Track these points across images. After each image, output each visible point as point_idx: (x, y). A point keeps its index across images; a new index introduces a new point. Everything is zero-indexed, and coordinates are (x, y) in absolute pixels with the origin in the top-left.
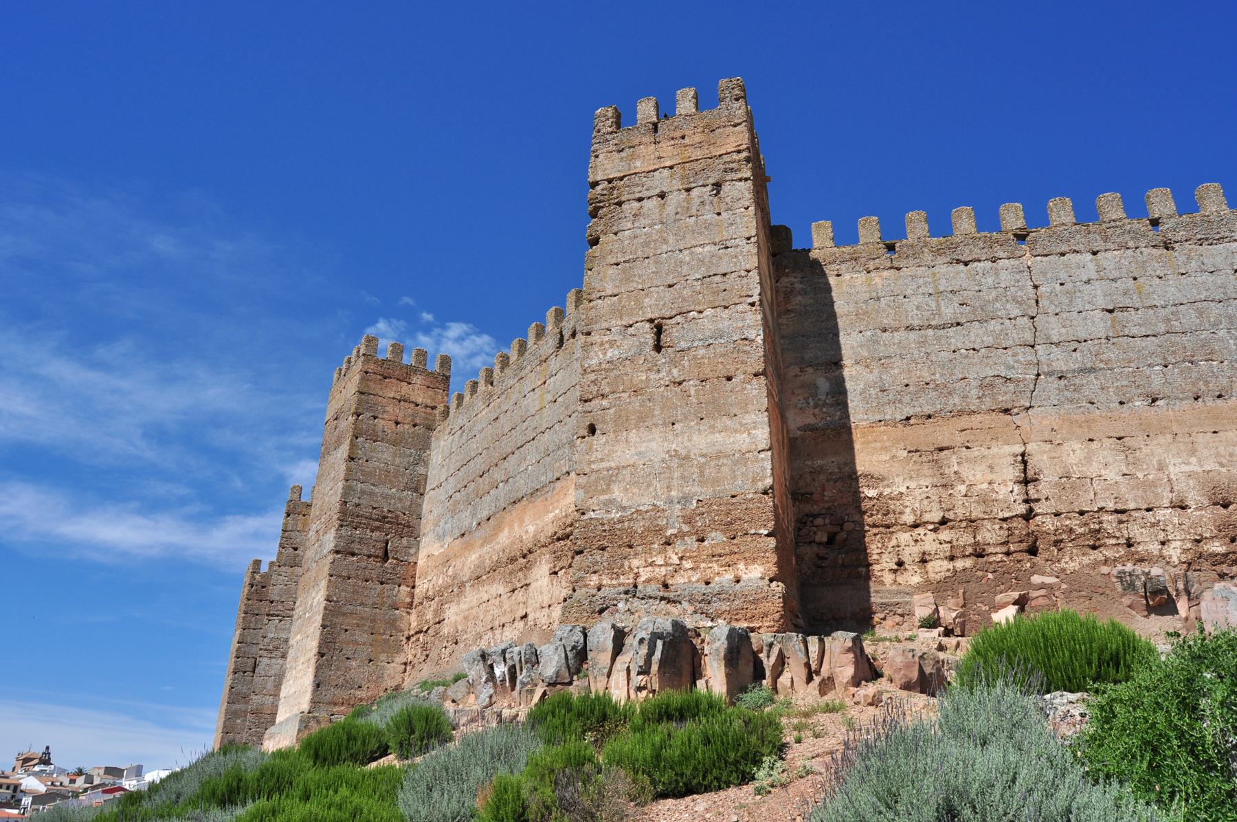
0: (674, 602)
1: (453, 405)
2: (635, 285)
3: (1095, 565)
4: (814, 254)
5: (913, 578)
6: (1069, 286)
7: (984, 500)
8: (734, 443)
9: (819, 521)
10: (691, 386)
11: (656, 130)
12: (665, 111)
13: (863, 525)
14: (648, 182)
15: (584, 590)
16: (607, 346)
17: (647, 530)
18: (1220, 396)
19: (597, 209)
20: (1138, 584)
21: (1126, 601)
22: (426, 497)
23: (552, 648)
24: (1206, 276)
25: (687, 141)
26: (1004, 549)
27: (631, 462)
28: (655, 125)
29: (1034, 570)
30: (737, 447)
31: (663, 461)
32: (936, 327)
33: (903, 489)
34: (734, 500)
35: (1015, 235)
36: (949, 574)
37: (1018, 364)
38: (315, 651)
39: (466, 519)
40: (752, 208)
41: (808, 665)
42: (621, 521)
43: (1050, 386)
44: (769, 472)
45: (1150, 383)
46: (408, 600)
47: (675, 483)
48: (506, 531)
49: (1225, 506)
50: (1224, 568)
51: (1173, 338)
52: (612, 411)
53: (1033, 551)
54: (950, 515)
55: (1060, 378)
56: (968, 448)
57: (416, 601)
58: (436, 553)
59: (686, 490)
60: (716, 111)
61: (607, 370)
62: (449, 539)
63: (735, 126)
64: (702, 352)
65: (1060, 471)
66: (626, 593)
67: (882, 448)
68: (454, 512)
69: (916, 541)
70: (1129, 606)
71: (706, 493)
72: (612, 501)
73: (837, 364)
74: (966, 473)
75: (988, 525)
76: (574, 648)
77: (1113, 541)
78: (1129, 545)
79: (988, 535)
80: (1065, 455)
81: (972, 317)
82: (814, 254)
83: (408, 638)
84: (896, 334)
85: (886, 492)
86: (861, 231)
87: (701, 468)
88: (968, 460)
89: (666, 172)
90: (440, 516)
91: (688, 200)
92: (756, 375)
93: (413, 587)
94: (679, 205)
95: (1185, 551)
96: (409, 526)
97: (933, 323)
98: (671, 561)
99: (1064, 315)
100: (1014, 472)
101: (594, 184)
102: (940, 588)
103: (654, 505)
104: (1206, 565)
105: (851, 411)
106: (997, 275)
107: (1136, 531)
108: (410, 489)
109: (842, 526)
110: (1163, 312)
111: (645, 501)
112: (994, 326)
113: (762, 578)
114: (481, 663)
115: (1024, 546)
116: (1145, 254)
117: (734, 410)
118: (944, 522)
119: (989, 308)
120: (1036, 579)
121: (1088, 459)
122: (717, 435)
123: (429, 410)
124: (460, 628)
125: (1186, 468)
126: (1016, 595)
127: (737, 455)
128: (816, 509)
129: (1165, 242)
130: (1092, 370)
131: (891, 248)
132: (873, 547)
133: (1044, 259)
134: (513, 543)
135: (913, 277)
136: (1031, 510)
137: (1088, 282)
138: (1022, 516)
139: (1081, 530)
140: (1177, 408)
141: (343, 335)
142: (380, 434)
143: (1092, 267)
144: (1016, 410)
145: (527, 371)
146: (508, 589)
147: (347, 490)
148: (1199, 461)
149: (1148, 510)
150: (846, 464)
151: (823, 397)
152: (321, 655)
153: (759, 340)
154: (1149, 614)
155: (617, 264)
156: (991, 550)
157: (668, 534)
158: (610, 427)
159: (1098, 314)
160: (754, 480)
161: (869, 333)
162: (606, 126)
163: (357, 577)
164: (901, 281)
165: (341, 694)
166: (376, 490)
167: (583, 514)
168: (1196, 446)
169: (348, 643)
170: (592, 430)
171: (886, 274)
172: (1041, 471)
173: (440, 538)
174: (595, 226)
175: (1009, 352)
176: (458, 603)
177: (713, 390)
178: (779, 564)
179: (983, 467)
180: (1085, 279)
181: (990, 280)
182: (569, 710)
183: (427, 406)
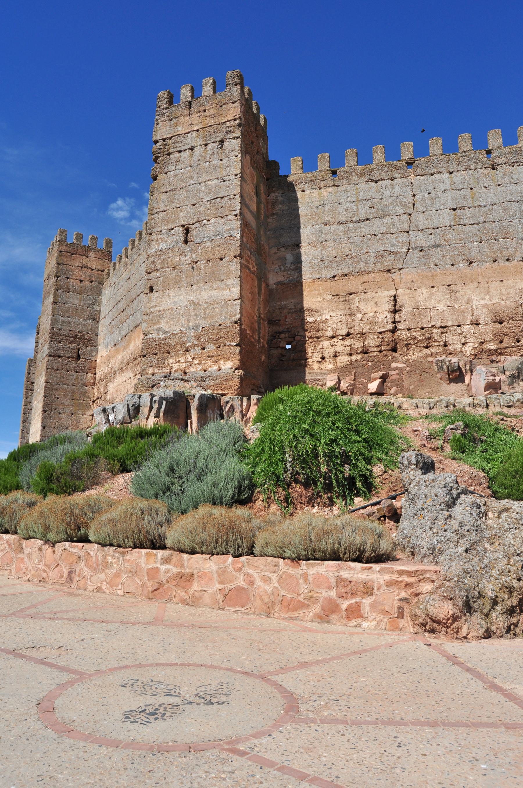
0: (188, 381)
1: (112, 268)
3: (426, 356)
4: (290, 179)
5: (329, 365)
6: (433, 194)
7: (371, 322)
8: (222, 296)
9: (282, 336)
10: (202, 264)
11: (190, 107)
12: (195, 93)
13: (305, 337)
14: (185, 141)
15: (146, 376)
16: (160, 241)
17: (177, 343)
18: (508, 260)
19: (157, 158)
20: (445, 367)
21: (439, 376)
22: (100, 323)
23: (122, 405)
24: (513, 187)
25: (207, 113)
26: (379, 349)
27: (170, 307)
29: (393, 360)
30: (223, 298)
31: (186, 306)
32: (355, 222)
33: (328, 317)
34: (220, 327)
35: (407, 163)
36: (348, 363)
37: (397, 244)
38: (41, 409)
39: (117, 337)
41: (242, 411)
42: (164, 339)
43: (415, 255)
44: (238, 311)
45: (470, 253)
46: (92, 381)
47: (192, 318)
48: (133, 343)
49: (501, 323)
50: (494, 357)
51: (488, 225)
53: (394, 350)
54: (352, 331)
55: (421, 251)
56: (365, 293)
57: (97, 382)
58: (105, 355)
59: (197, 322)
60: (223, 93)
61: (160, 255)
62: (109, 347)
63: (233, 103)
64: (208, 244)
65: (413, 305)
66: (165, 377)
67: (318, 294)
68: (112, 332)
69: (333, 345)
70: (440, 379)
71: (206, 323)
72: (160, 329)
73: (298, 245)
74: (363, 308)
75: (371, 336)
76: (133, 405)
77: (437, 344)
78: (446, 346)
79: (371, 341)
80: (417, 296)
81: (376, 215)
82: (290, 179)
83: (93, 402)
84: (332, 226)
85: (319, 318)
86: (319, 163)
87: (205, 309)
88: (365, 300)
89: (194, 134)
90: (106, 334)
91: (205, 152)
92: (235, 257)
93: (95, 374)
94: (200, 155)
95: (474, 348)
96: (91, 340)
97: (354, 219)
98: (188, 360)
99: (427, 213)
100: (389, 306)
101: (156, 142)
102: (342, 371)
104: (485, 356)
105: (303, 273)
106: (393, 188)
107: (450, 338)
108: (91, 319)
109: (294, 338)
110: (484, 209)
111: (176, 328)
112: (388, 220)
113: (231, 368)
114: (103, 414)
115: (389, 347)
116: (480, 173)
117: (223, 277)
118: (348, 335)
119: (386, 209)
120: (394, 365)
121: (430, 298)
122: (214, 291)
123: (100, 272)
124: (114, 396)
125: (482, 302)
126: (381, 374)
127: (223, 302)
128: (281, 329)
129: (493, 165)
130: (439, 245)
131: (334, 173)
132: (309, 349)
133: (421, 178)
134: (135, 349)
135: (345, 191)
136: (396, 327)
137: (444, 192)
138: (390, 331)
139: (421, 338)
140: (483, 267)
141: (96, 210)
142: (71, 287)
143: (448, 182)
144: (393, 271)
145: (141, 250)
147: (54, 321)
148: (490, 298)
149: (458, 326)
150: (298, 303)
151: (289, 265)
152: (44, 411)
154: (450, 383)
155: (166, 192)
156: (371, 349)
157: (187, 346)
159: (447, 211)
160: (231, 316)
161: (317, 226)
162: (163, 104)
163: (62, 369)
164: (338, 194)
166: (71, 320)
167: (146, 335)
168: (490, 289)
169: (59, 405)
170: (151, 289)
171: (330, 189)
172: (403, 305)
173: (106, 346)
174: (156, 168)
175: (394, 236)
177: (213, 266)
178: (241, 361)
179: (372, 303)
180: (443, 190)
181: (388, 192)
182: (112, 435)
183: (98, 270)
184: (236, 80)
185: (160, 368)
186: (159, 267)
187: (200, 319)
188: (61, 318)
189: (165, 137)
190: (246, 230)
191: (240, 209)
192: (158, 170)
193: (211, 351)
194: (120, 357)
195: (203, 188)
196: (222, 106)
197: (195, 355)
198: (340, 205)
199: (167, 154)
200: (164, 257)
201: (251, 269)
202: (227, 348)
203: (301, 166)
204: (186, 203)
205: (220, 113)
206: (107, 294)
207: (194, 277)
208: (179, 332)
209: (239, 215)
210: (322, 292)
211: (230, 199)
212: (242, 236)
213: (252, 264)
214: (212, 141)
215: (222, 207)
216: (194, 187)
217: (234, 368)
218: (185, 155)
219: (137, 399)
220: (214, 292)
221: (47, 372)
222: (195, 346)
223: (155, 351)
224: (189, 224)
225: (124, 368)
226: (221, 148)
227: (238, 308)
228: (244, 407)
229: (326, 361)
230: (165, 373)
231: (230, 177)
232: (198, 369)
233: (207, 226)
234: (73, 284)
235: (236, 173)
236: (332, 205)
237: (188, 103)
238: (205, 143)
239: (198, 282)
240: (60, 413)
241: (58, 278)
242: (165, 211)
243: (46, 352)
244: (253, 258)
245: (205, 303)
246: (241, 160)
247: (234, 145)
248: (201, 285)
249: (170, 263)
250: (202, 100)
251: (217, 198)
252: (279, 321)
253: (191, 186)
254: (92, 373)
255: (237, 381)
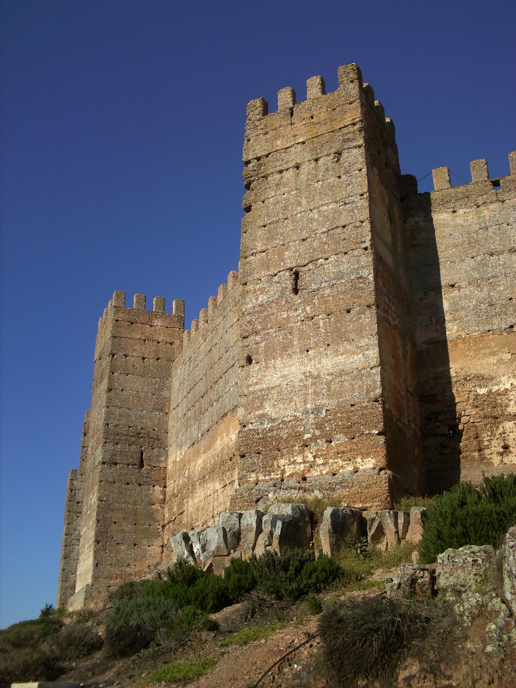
2: (277, 241)
8: (352, 362)
11: (292, 114)
17: (290, 435)
22: (171, 415)
27: (278, 383)
28: (291, 109)
33: (508, 386)
34: (353, 408)
38: (93, 539)
40: (364, 170)
41: (397, 532)
42: (271, 430)
44: (379, 383)
46: (161, 497)
47: (310, 397)
52: (263, 344)
57: (167, 498)
59: (318, 402)
63: (351, 104)
64: (328, 291)
68: (187, 426)
71: (330, 403)
83: (164, 526)
85: (495, 388)
86: (473, 173)
91: (316, 169)
93: (165, 487)
94: (309, 173)
101: (248, 163)
103: (295, 416)
113: (374, 468)
117: (352, 336)
122: (340, 357)
127: (355, 372)
131: (496, 184)
142: (131, 368)
145: (227, 311)
146: (221, 486)
147: (109, 415)
152: (97, 542)
153: (371, 278)
155: (265, 226)
158: (262, 357)
160: (368, 391)
161: (479, 258)
163: (121, 481)
165: (115, 570)
167: (245, 426)
171: (492, 206)
174: (249, 197)
176: (192, 498)
184: (351, 76)
185: (267, 473)
186: (259, 327)
187: (323, 398)
188: (118, 410)
189: (259, 155)
190: (381, 268)
191: (371, 240)
192: (252, 198)
193: (342, 444)
194: (200, 462)
195: (316, 216)
196: (334, 109)
197: (317, 451)
198: (510, 227)
199: (263, 177)
200: (266, 313)
201: (392, 322)
202: (365, 438)
203: (448, 178)
204: (293, 238)
205: (333, 118)
206: (180, 374)
207: (310, 339)
208: (292, 418)
209: (369, 248)
210: (495, 350)
211: (355, 227)
212: (376, 277)
213: (392, 315)
214: (325, 154)
215: (344, 239)
216: (302, 216)
217: (378, 468)
218: (289, 175)
219: (237, 519)
220: (341, 359)
221: (100, 485)
222: (317, 439)
223: (259, 447)
224: (299, 266)
225: (207, 477)
226: (337, 161)
227: (378, 378)
228: (400, 527)
229: (510, 452)
230: (273, 479)
231: (353, 198)
232: (324, 472)
233: (325, 266)
234: (133, 364)
235: (361, 192)
236: (498, 227)
237: (288, 111)
238: (315, 157)
239: (317, 345)
240: (118, 544)
241: (113, 356)
242: (264, 252)
243: (100, 458)
244: (393, 308)
245: (328, 375)
246: (367, 175)
247: (356, 157)
248: (321, 349)
249: (274, 321)
250: (307, 103)
251: (336, 228)
252: (435, 395)
253: (299, 215)
254: (160, 487)
255: (385, 486)
